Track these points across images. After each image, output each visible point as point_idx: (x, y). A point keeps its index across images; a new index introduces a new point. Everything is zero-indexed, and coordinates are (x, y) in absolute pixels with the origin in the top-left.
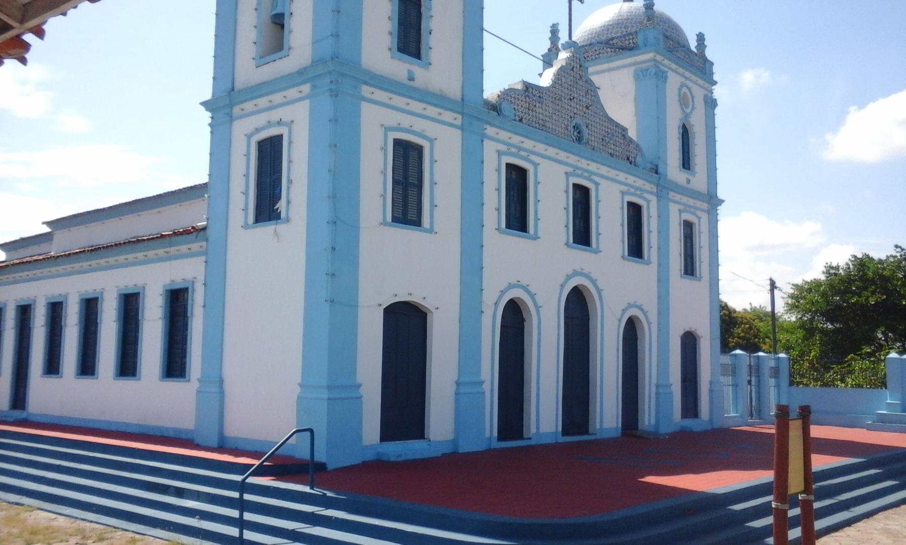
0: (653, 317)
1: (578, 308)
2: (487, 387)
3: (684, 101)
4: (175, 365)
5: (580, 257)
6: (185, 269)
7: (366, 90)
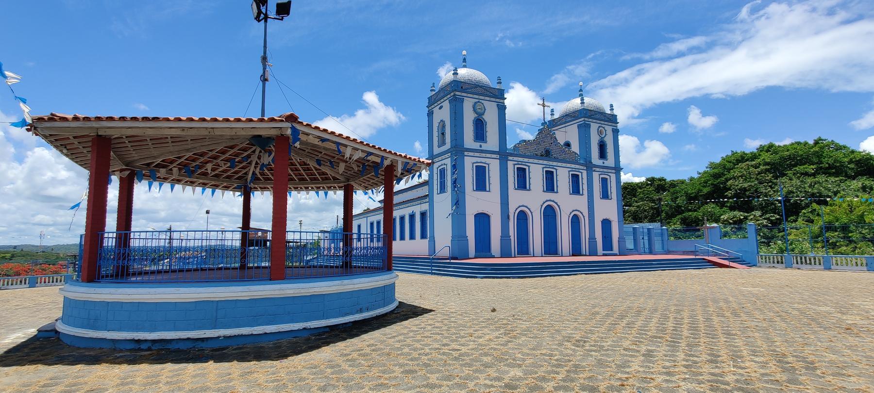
0: (586, 214)
1: (550, 214)
2: (512, 238)
3: (600, 133)
4: (372, 224)
5: (550, 196)
6: (425, 207)
7: (466, 153)
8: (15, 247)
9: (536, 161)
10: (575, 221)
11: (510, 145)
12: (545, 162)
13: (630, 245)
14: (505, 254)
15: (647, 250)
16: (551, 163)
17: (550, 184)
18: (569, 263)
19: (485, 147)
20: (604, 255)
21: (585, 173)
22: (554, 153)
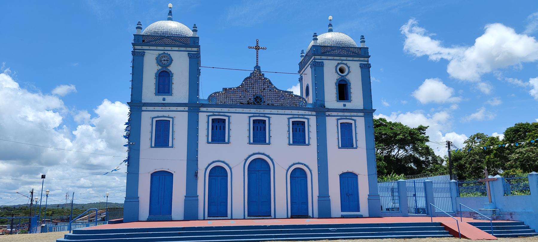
1: (259, 171)
8: (58, 206)
9: (240, 110)
10: (298, 176)
11: (204, 95)
16: (262, 111)
17: (259, 132)
18: (183, 229)
19: (169, 99)
20: (343, 217)
21: (313, 120)
22: (268, 98)
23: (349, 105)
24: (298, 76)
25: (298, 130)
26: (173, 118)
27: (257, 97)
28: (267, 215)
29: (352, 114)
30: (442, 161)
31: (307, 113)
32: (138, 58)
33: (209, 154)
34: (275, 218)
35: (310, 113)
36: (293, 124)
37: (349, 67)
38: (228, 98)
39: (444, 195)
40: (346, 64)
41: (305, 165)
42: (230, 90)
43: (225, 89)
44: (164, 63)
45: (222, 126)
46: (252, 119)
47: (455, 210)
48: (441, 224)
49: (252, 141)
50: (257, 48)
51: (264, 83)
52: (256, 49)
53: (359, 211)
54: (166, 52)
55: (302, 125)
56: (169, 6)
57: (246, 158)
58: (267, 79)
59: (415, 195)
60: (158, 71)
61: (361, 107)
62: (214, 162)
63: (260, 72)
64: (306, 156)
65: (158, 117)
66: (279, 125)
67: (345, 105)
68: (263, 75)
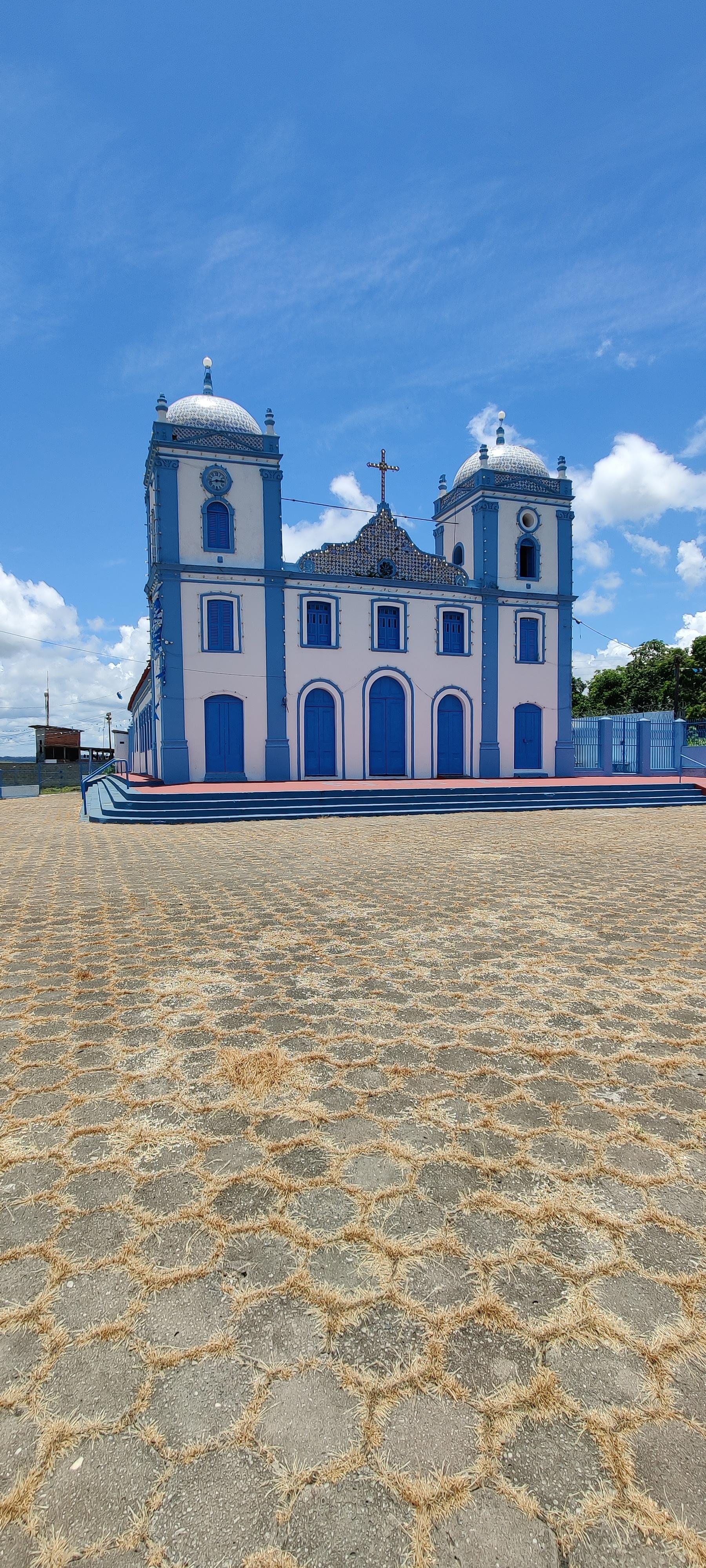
1: (387, 697)
7: (184, 576)
10: (450, 710)
12: (378, 589)
13: (588, 755)
14: (276, 770)
15: (633, 767)
16: (393, 590)
17: (389, 631)
19: (229, 560)
20: (517, 777)
21: (477, 611)
22: (403, 567)
23: (536, 587)
24: (433, 526)
25: (317, 619)
26: (238, 597)
27: (384, 563)
28: (400, 772)
29: (541, 603)
30: (583, 687)
31: (468, 597)
32: (161, 472)
33: (304, 666)
34: (413, 779)
35: (472, 598)
36: (308, 608)
37: (538, 516)
38: (326, 563)
39: (663, 743)
40: (534, 510)
41: (462, 690)
42: (338, 549)
43: (327, 546)
44: (217, 484)
45: (392, 619)
46: (442, 610)
47: (678, 764)
48: (695, 786)
49: (376, 646)
50: (383, 468)
51: (397, 538)
52: (381, 469)
53: (540, 767)
54: (219, 464)
55: (326, 609)
56: (205, 364)
57: (407, 673)
58: (402, 530)
59: (623, 743)
60: (206, 501)
61: (554, 591)
62: (312, 681)
63: (389, 515)
64: (464, 674)
65: (211, 594)
66: (422, 618)
67: (529, 587)
68: (395, 521)
